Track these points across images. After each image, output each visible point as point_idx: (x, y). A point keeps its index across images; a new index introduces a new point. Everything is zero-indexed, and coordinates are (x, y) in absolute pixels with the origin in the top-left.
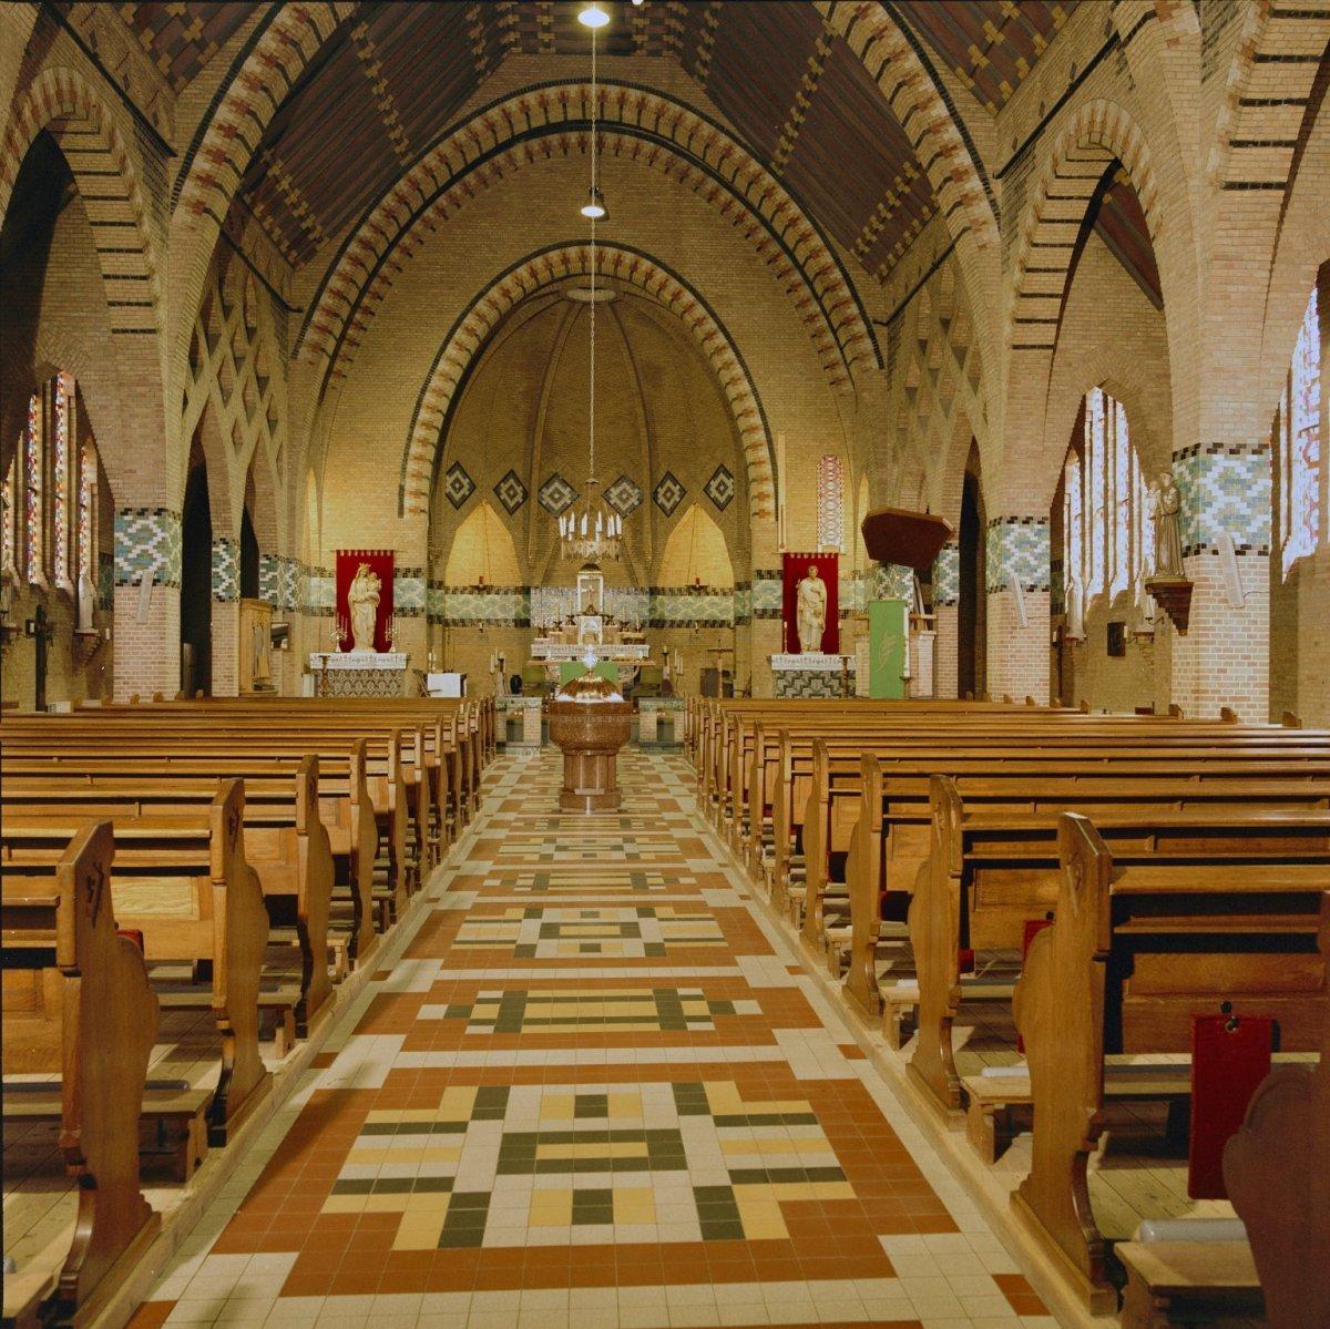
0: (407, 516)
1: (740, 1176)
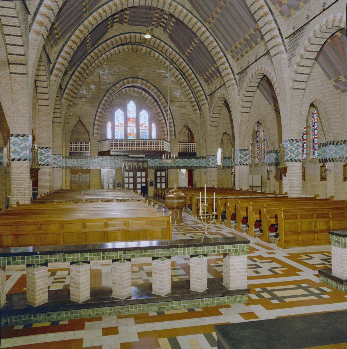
0: (95, 135)
1: (139, 272)
